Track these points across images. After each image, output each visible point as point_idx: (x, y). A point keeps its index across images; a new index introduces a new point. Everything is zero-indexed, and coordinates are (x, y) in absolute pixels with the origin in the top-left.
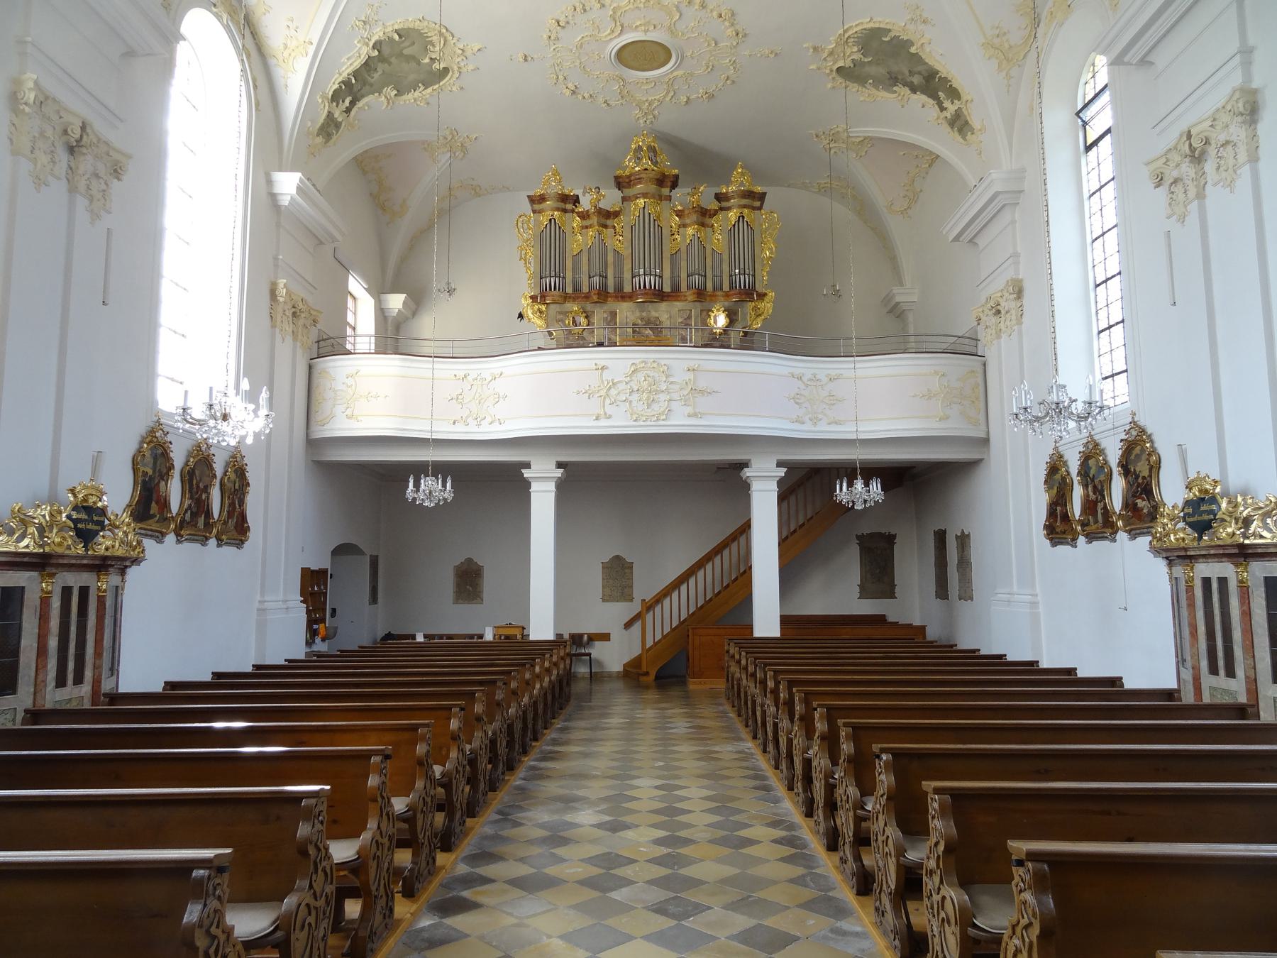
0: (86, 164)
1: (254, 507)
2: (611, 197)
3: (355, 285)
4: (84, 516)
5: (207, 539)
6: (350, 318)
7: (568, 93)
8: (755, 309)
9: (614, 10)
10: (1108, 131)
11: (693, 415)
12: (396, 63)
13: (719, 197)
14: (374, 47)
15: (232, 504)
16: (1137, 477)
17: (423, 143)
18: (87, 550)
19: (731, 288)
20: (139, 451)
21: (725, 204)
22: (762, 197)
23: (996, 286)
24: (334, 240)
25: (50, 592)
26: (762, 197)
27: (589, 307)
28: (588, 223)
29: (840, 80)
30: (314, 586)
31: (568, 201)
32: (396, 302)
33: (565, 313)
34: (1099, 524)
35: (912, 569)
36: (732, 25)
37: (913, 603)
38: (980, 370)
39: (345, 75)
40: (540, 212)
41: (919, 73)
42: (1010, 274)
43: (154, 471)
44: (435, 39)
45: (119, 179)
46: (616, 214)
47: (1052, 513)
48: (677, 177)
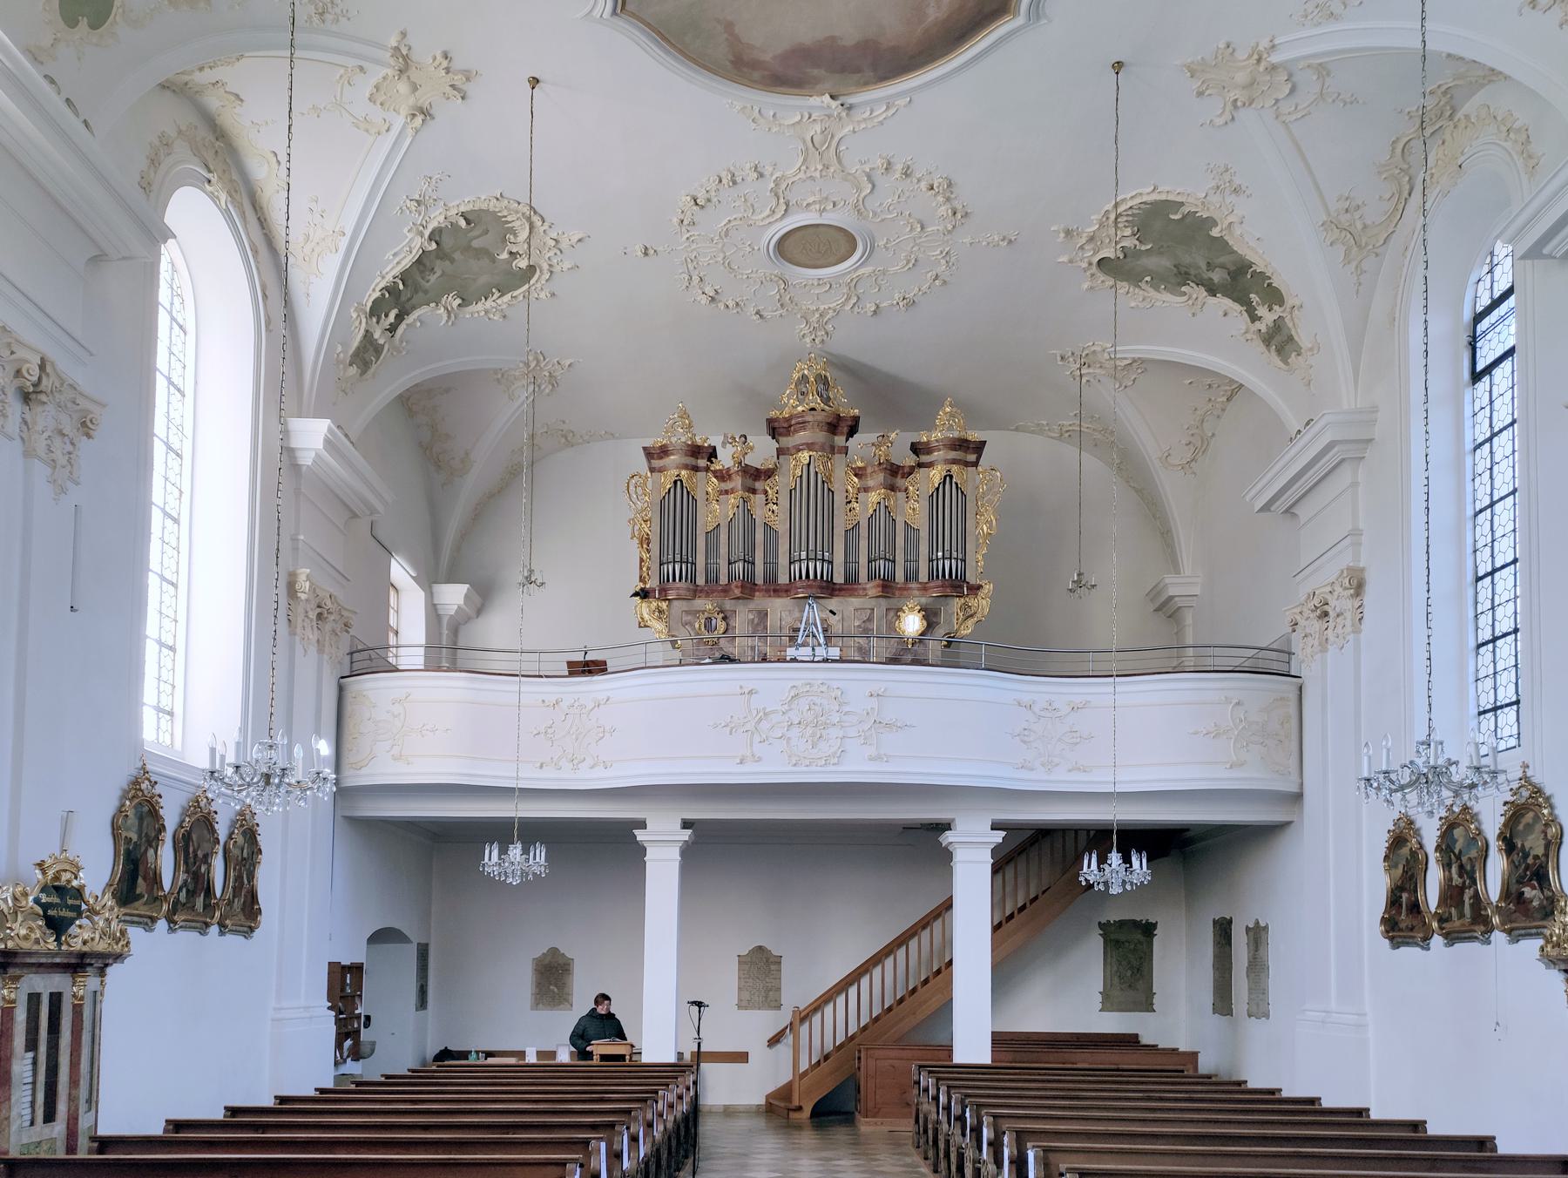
0: (45, 417)
1: (267, 881)
2: (762, 450)
3: (400, 572)
4: (57, 900)
5: (207, 925)
6: (392, 622)
7: (704, 300)
8: (965, 607)
9: (777, 183)
10: (1510, 352)
11: (878, 758)
12: (459, 260)
13: (916, 449)
14: (430, 239)
15: (239, 878)
16: (1526, 855)
17: (496, 371)
18: (60, 944)
19: (931, 577)
20: (120, 809)
21: (925, 459)
22: (979, 447)
23: (1325, 577)
24: (373, 511)
25: (13, 1002)
26: (979, 447)
27: (728, 605)
28: (728, 486)
29: (1101, 277)
30: (345, 985)
31: (702, 454)
32: (453, 596)
33: (695, 613)
34: (1465, 918)
35: (1180, 967)
36: (948, 199)
37: (1178, 1018)
38: (1293, 696)
39: (389, 278)
40: (661, 470)
41: (1222, 266)
42: (1346, 560)
43: (140, 837)
44: (516, 224)
45: (89, 436)
46: (769, 474)
47: (1393, 902)
48: (856, 420)
